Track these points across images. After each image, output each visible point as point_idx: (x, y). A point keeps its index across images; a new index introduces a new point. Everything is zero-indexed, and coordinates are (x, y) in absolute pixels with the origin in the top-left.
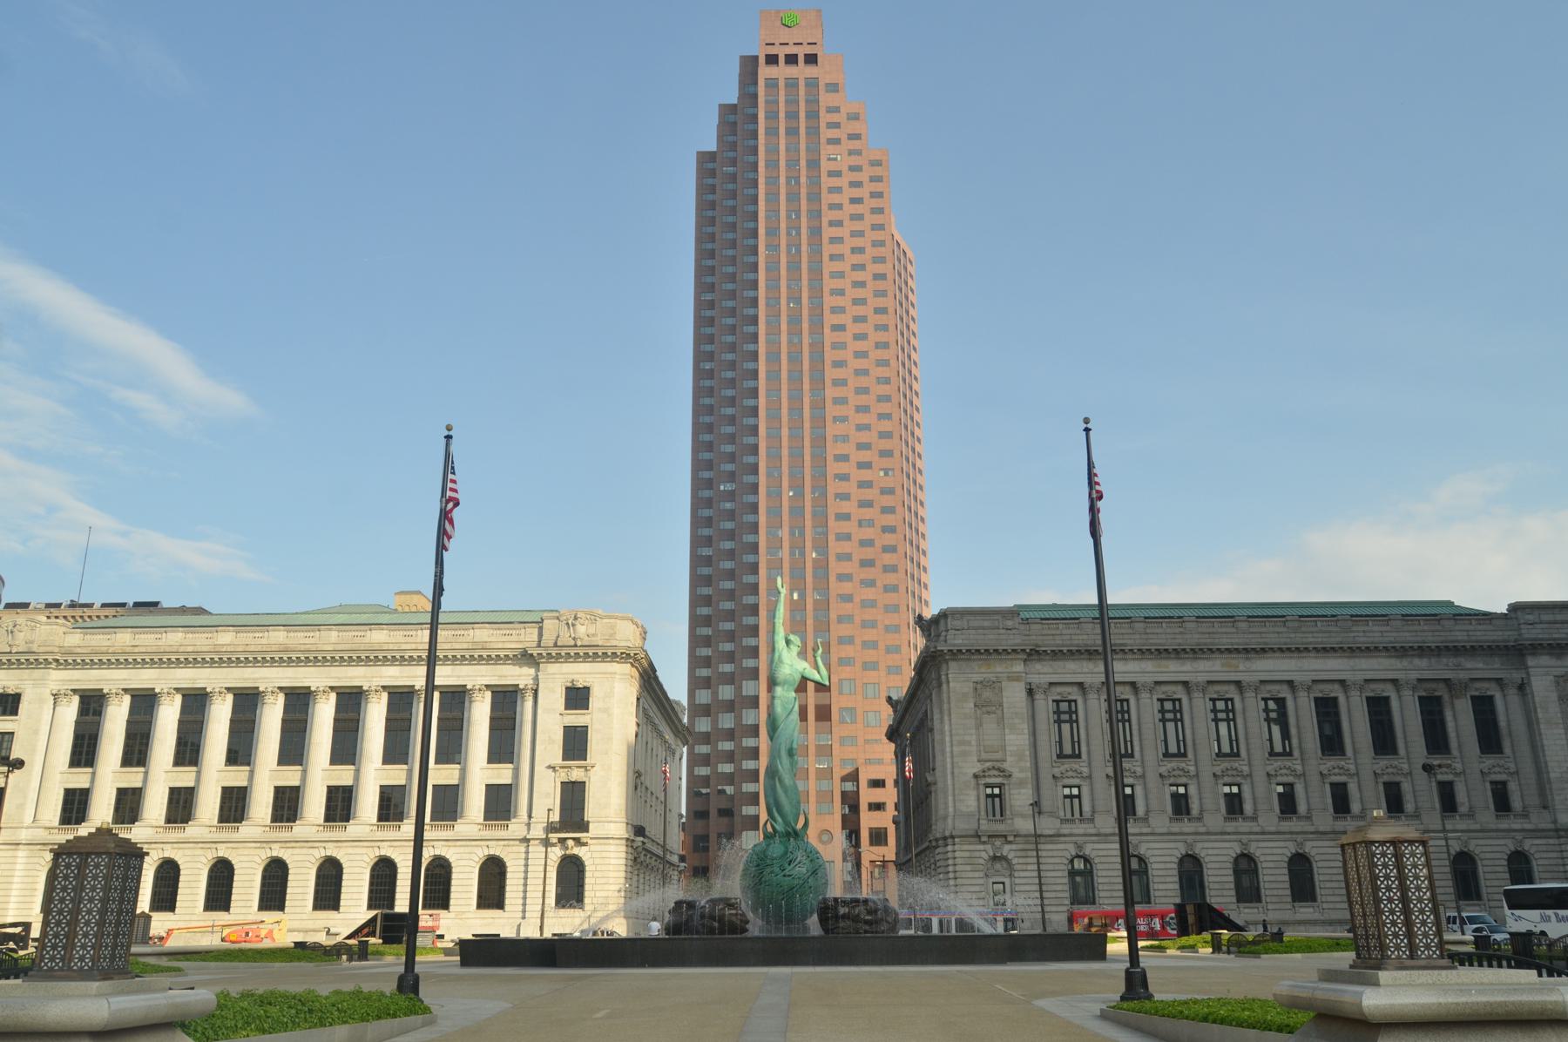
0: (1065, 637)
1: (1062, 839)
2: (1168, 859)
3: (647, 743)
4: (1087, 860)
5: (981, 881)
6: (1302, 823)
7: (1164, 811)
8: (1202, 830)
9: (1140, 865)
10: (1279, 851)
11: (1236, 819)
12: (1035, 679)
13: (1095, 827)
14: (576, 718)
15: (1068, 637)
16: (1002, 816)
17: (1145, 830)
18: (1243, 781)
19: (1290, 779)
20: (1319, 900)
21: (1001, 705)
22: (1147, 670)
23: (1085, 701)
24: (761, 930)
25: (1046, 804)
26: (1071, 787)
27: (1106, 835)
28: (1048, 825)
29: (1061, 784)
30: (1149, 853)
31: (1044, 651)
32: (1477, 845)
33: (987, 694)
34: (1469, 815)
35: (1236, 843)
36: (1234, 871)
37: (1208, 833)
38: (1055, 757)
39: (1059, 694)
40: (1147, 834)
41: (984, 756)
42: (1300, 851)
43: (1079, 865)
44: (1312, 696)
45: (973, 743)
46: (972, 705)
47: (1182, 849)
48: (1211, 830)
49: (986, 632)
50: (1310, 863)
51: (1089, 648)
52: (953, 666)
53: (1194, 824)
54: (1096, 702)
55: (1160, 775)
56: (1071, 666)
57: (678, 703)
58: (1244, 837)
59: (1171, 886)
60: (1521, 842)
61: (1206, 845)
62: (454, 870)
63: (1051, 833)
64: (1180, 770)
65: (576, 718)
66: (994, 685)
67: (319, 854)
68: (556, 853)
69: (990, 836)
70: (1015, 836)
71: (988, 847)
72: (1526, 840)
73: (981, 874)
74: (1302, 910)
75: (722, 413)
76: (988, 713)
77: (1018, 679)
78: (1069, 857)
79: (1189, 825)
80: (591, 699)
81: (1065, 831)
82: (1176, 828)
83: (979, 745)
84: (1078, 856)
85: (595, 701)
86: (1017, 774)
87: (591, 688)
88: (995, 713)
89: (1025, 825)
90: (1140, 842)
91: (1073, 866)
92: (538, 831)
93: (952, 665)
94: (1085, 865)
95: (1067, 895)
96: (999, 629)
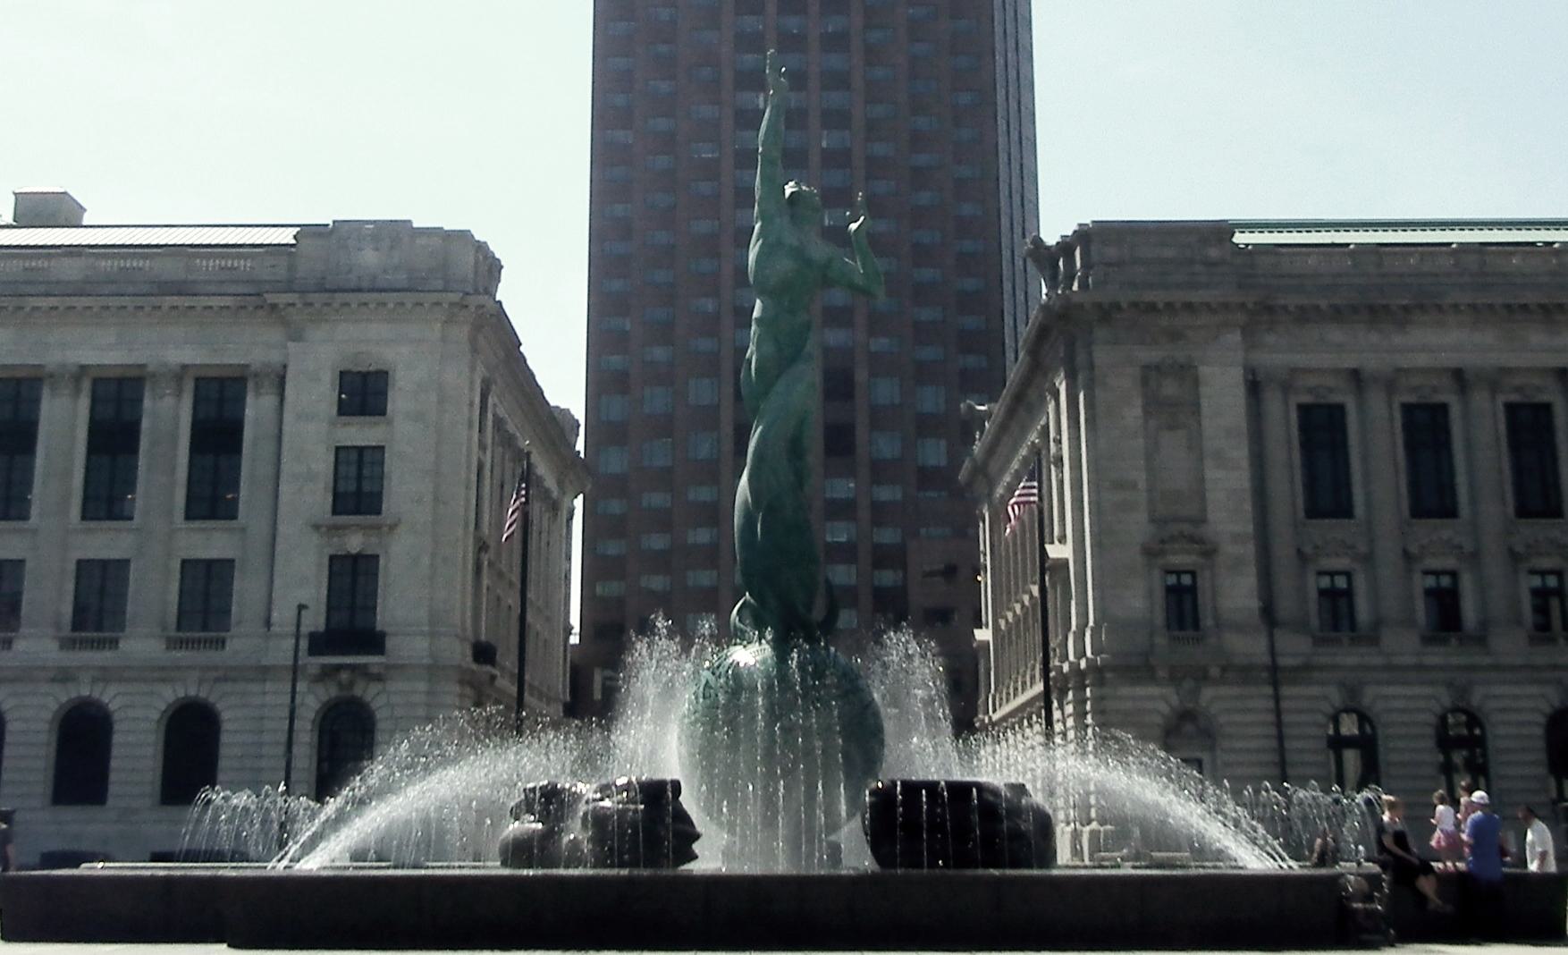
3: (502, 487)
4: (1363, 718)
7: (1518, 622)
14: (360, 433)
19: (1450, 563)
23: (1361, 408)
24: (727, 854)
25: (1286, 606)
26: (1332, 574)
33: (1170, 388)
37: (1496, 668)
38: (1301, 514)
39: (1518, 389)
43: (1349, 727)
44: (1501, 399)
57: (566, 412)
61: (1390, 690)
62: (116, 727)
65: (360, 433)
67: (169, 694)
68: (312, 701)
78: (1330, 711)
80: (390, 394)
81: (1323, 660)
83: (1150, 490)
84: (1348, 711)
85: (398, 401)
86: (1229, 549)
87: (390, 373)
89: (1251, 647)
91: (1337, 730)
92: (281, 653)
93: (1101, 333)
94: (1361, 727)
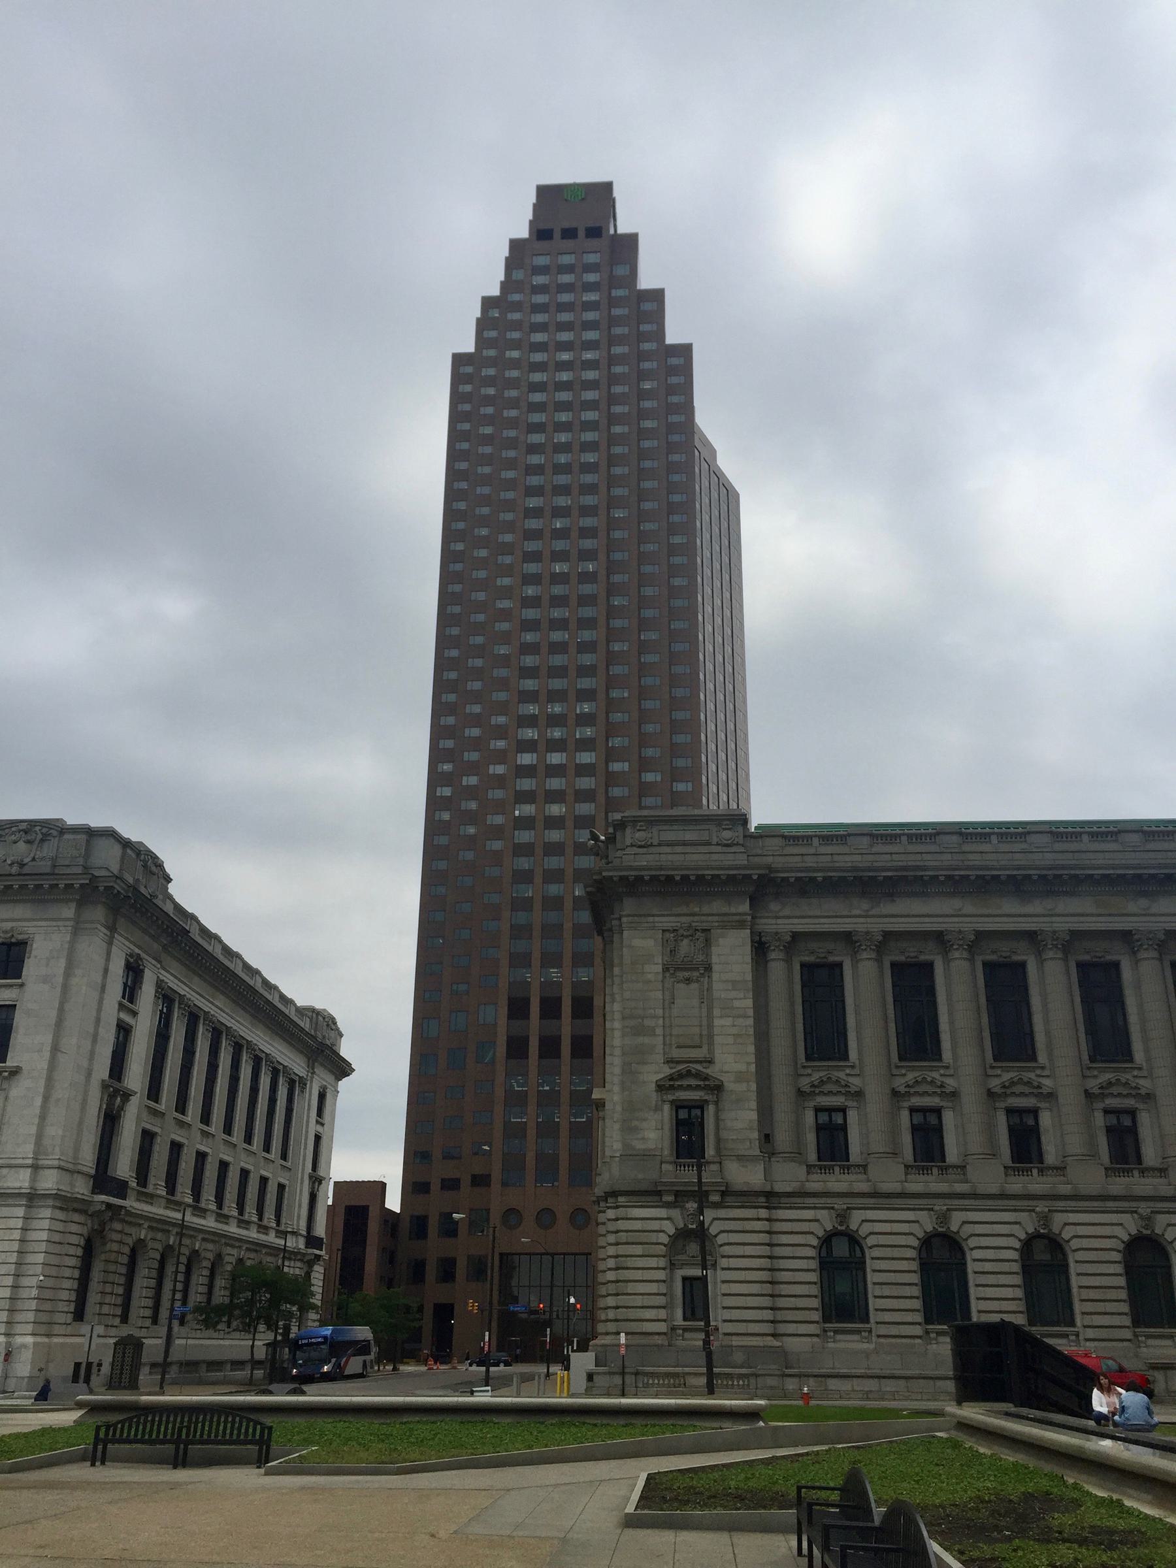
0: (822, 859)
1: (810, 1201)
2: (902, 1240)
4: (854, 1241)
5: (661, 1275)
6: (852, 1177)
8: (1065, 1189)
9: (852, 1250)
10: (904, 1228)
11: (1129, 1172)
12: (768, 925)
13: (869, 1181)
15: (829, 858)
16: (284, 1157)
17: (960, 1188)
18: (1140, 1106)
20: (872, 1320)
21: (708, 968)
22: (964, 912)
27: (889, 1195)
28: (788, 1176)
29: (812, 1104)
30: (865, 1230)
31: (783, 879)
32: (1169, 1225)
34: (1057, 1168)
35: (825, 1212)
36: (1023, 1266)
37: (975, 1196)
40: (962, 1196)
41: (676, 1053)
42: (1145, 1232)
45: (659, 1031)
46: (659, 968)
47: (1028, 1224)
48: (981, 1189)
49: (688, 849)
50: (1065, 1255)
51: (861, 874)
52: (629, 906)
53: (1050, 1179)
54: (965, 965)
55: (1086, 1091)
56: (833, 905)
58: (1143, 1204)
59: (1009, 1293)
60: (1149, 1219)
63: (789, 1189)
64: (927, 1082)
66: (705, 937)
69: (677, 1194)
70: (723, 1194)
71: (676, 1213)
72: (1160, 1217)
73: (662, 1262)
74: (1151, 1342)
75: (454, 507)
76: (688, 981)
77: (741, 925)
79: (1041, 1179)
82: (1016, 1185)
88: (698, 981)
90: (848, 1208)
95: (815, 1303)
96: (710, 844)
